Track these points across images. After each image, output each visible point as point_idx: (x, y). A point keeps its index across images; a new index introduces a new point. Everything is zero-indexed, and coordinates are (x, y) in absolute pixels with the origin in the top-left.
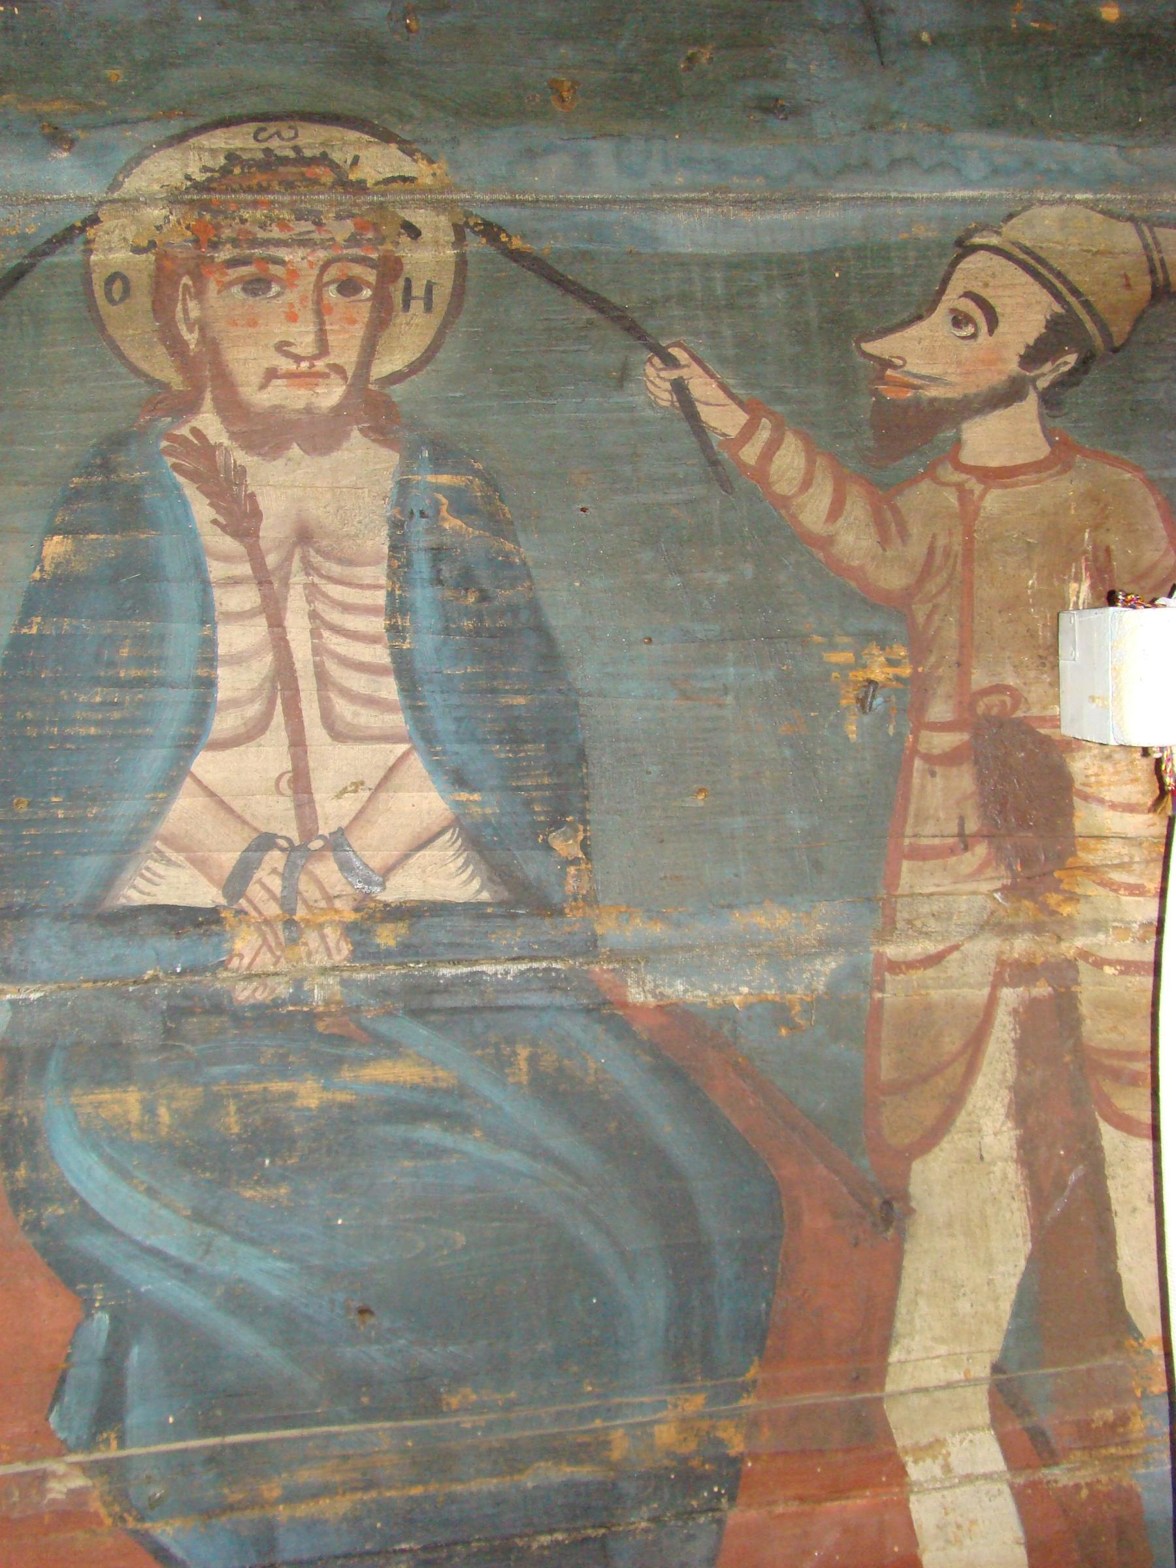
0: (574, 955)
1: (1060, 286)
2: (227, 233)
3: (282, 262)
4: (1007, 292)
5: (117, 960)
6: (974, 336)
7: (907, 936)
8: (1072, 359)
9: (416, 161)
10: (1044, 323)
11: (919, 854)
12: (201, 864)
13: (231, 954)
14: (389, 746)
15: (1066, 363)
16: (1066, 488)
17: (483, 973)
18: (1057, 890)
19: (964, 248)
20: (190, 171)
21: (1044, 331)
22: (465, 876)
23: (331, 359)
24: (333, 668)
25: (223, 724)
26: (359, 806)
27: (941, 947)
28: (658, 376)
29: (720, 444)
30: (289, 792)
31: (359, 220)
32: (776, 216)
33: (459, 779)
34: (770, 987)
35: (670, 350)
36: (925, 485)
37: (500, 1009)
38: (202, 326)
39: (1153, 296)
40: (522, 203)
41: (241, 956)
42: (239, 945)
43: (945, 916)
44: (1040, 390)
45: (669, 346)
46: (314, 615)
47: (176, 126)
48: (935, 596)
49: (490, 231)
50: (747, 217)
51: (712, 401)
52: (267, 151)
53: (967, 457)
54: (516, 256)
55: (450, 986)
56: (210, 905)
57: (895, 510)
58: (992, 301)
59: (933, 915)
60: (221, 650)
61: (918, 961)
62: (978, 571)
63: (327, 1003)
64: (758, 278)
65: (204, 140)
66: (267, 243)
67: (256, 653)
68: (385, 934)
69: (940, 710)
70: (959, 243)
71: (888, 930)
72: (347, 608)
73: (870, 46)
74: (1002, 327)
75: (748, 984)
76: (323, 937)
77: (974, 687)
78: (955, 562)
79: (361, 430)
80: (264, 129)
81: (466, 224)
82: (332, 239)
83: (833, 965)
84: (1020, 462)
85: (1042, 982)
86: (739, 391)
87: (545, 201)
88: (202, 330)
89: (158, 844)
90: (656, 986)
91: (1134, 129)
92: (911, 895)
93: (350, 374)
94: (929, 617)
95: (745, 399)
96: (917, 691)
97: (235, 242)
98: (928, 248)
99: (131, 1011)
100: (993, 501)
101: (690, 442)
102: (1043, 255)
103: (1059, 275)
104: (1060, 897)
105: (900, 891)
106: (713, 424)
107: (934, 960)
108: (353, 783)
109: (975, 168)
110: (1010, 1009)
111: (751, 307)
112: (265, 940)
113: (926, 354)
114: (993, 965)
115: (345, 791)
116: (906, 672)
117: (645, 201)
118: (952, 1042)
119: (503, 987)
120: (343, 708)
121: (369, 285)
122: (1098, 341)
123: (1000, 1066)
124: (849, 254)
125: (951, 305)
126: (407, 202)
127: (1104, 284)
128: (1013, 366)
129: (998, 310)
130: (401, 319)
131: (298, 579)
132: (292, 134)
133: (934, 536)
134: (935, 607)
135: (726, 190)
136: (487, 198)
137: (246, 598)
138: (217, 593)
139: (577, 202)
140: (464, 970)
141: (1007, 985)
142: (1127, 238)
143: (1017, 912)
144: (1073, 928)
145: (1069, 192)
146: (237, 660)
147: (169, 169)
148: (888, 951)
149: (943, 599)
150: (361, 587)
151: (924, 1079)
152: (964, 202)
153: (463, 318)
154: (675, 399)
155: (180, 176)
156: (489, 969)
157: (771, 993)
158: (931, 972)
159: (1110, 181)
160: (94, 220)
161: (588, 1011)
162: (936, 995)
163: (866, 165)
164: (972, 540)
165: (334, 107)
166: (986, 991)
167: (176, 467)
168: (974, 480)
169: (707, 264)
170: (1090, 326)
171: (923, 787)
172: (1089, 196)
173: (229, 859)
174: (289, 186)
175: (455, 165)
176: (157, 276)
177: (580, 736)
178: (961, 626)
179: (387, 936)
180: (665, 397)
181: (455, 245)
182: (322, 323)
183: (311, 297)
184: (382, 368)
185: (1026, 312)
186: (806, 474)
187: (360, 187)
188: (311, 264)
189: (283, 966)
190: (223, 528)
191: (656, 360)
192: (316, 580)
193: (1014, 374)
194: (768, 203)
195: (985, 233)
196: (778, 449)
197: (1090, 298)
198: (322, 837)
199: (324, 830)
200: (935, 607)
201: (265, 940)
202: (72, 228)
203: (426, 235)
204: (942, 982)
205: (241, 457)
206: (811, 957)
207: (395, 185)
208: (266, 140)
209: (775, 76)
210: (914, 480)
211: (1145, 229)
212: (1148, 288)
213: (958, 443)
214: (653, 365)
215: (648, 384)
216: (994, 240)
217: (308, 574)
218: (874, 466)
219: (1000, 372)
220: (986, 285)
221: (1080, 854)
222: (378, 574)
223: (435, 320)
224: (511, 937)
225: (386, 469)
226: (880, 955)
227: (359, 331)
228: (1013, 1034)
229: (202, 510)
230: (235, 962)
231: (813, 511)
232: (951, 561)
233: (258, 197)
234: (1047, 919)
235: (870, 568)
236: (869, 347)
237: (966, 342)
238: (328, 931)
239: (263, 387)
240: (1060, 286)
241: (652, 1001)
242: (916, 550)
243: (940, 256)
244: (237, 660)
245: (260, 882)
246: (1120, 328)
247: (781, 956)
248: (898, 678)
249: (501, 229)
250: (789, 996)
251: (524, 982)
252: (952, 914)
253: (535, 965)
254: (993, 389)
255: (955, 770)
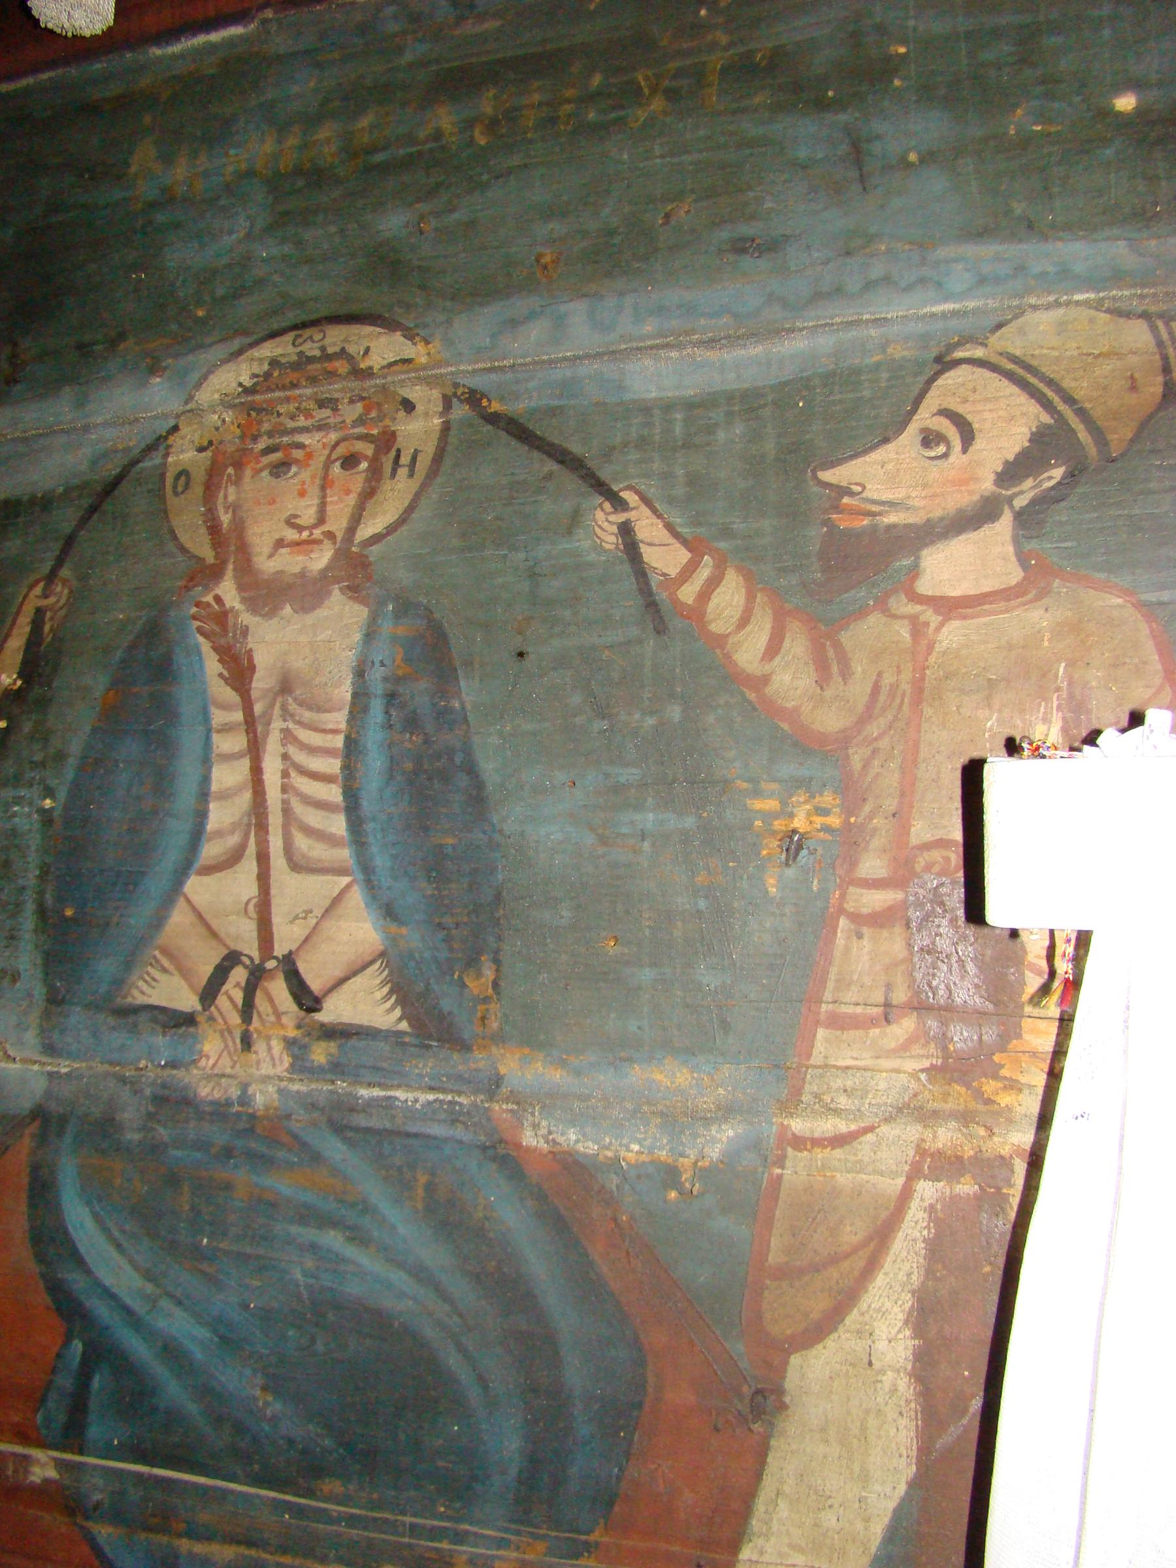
0: (476, 1092)
1: (1050, 394)
2: (266, 426)
3: (300, 446)
4: (989, 406)
5: (122, 1048)
6: (945, 456)
7: (813, 1111)
8: (1058, 473)
9: (415, 344)
10: (1028, 436)
11: (838, 1022)
12: (185, 973)
13: (202, 1055)
14: (336, 878)
15: (1050, 478)
16: (1038, 618)
17: (397, 1099)
18: (995, 1077)
19: (944, 363)
20: (242, 379)
21: (1027, 444)
22: (388, 1004)
23: (325, 528)
24: (298, 807)
25: (210, 851)
26: (307, 932)
27: (853, 1127)
28: (607, 520)
29: (660, 584)
30: (254, 916)
31: (367, 402)
32: (743, 352)
33: (389, 912)
34: (661, 1148)
35: (621, 494)
36: (874, 619)
37: (408, 1135)
38: (235, 508)
39: (1164, 396)
40: (502, 369)
41: (208, 1057)
42: (207, 1048)
43: (859, 1093)
44: (1017, 509)
45: (621, 490)
46: (285, 757)
47: (236, 343)
48: (876, 739)
49: (474, 398)
50: (711, 355)
51: (657, 541)
52: (301, 353)
53: (924, 586)
54: (493, 419)
55: (372, 1103)
56: (188, 1009)
57: (837, 645)
58: (969, 417)
59: (845, 1091)
60: (214, 787)
61: (825, 1139)
62: (928, 711)
63: (267, 1108)
64: (717, 415)
65: (256, 353)
66: (295, 431)
67: (239, 790)
68: (319, 1051)
69: (872, 865)
70: (938, 359)
71: (791, 1103)
72: (313, 750)
73: (854, 174)
74: (978, 444)
75: (640, 1143)
76: (270, 1049)
77: (914, 840)
78: (902, 700)
79: (341, 589)
80: (300, 336)
81: (455, 395)
82: (344, 421)
83: (731, 1133)
84: (986, 589)
85: (968, 1178)
86: (684, 531)
87: (521, 365)
88: (234, 512)
89: (157, 953)
90: (550, 1133)
91: (1150, 219)
92: (826, 1066)
93: (339, 539)
94: (866, 765)
95: (689, 537)
96: (850, 841)
97: (270, 434)
98: (901, 367)
99: (125, 1093)
100: (952, 635)
101: (630, 584)
102: (1035, 363)
103: (1050, 383)
104: (1000, 1085)
105: (812, 1061)
106: (655, 565)
107: (839, 1141)
108: (304, 911)
109: (959, 278)
110: (926, 1204)
111: (708, 444)
112: (226, 1046)
113: (889, 478)
114: (911, 1153)
115: (296, 917)
116: (835, 821)
117: (613, 352)
118: (853, 1233)
119: (411, 1113)
120: (302, 842)
121: (366, 458)
122: (1092, 451)
123: (906, 1267)
124: (817, 382)
125: (923, 425)
126: (403, 381)
127: (1105, 388)
128: (987, 485)
129: (975, 426)
130: (387, 485)
131: (277, 725)
132: (320, 336)
133: (880, 675)
134: (875, 752)
135: (693, 331)
136: (470, 368)
137: (234, 743)
138: (215, 737)
139: (550, 362)
140: (377, 1092)
141: (926, 1178)
142: (1138, 335)
143: (945, 1096)
144: (1010, 1121)
145: (1066, 294)
146: (224, 796)
147: (232, 377)
148: (793, 1124)
149: (884, 743)
150: (324, 731)
151: (816, 1268)
152: (944, 316)
153: (439, 480)
154: (620, 541)
155: (234, 385)
156: (400, 1094)
157: (663, 1154)
158: (838, 1153)
159: (1117, 277)
160: (175, 429)
161: (484, 1148)
162: (843, 1179)
163: (838, 291)
164: (923, 679)
165: (355, 308)
166: (901, 1181)
167: (200, 631)
168: (930, 612)
169: (668, 407)
170: (1083, 435)
171: (847, 949)
172: (1093, 296)
173: (206, 970)
174: (313, 380)
175: (448, 342)
176: (211, 469)
177: (500, 877)
178: (903, 770)
179: (320, 1053)
180: (611, 540)
181: (441, 414)
182: (324, 497)
183: (320, 473)
184: (366, 531)
185: (1008, 424)
186: (744, 612)
187: (368, 373)
188: (324, 445)
189: (238, 1070)
190: (226, 680)
191: (607, 506)
192: (291, 725)
193: (987, 494)
194: (733, 340)
195: (968, 346)
196: (718, 585)
197: (1088, 405)
198: (276, 958)
199: (280, 950)
200: (875, 752)
201: (226, 1046)
202: (160, 437)
203: (420, 408)
204: (849, 1165)
205: (246, 618)
206: (707, 1121)
207: (395, 368)
208: (301, 344)
209: (753, 217)
210: (862, 613)
211: (1160, 324)
212: (1159, 390)
213: (914, 572)
214: (603, 510)
215: (597, 529)
216: (979, 353)
217: (285, 720)
218: (819, 601)
219: (971, 493)
220: (965, 401)
221: (1026, 1036)
222: (339, 719)
223: (414, 484)
224: (425, 1066)
225: (356, 623)
226: (784, 1128)
227: (352, 499)
228: (925, 1232)
229: (212, 665)
230: (203, 1062)
231: (748, 652)
232: (898, 701)
233: (288, 393)
234: (981, 1107)
235: (806, 708)
236: (826, 476)
237: (935, 462)
238: (274, 1043)
239: (271, 556)
240: (1050, 394)
241: (544, 1146)
242: (859, 689)
243: (916, 375)
244: (224, 796)
245: (227, 993)
246: (1120, 436)
247: (679, 1119)
248: (826, 829)
249: (483, 395)
250: (681, 1159)
251: (430, 1112)
252: (867, 1092)
253: (441, 1097)
254: (960, 511)
255: (885, 933)
